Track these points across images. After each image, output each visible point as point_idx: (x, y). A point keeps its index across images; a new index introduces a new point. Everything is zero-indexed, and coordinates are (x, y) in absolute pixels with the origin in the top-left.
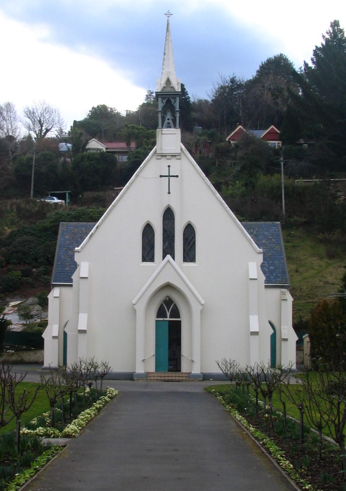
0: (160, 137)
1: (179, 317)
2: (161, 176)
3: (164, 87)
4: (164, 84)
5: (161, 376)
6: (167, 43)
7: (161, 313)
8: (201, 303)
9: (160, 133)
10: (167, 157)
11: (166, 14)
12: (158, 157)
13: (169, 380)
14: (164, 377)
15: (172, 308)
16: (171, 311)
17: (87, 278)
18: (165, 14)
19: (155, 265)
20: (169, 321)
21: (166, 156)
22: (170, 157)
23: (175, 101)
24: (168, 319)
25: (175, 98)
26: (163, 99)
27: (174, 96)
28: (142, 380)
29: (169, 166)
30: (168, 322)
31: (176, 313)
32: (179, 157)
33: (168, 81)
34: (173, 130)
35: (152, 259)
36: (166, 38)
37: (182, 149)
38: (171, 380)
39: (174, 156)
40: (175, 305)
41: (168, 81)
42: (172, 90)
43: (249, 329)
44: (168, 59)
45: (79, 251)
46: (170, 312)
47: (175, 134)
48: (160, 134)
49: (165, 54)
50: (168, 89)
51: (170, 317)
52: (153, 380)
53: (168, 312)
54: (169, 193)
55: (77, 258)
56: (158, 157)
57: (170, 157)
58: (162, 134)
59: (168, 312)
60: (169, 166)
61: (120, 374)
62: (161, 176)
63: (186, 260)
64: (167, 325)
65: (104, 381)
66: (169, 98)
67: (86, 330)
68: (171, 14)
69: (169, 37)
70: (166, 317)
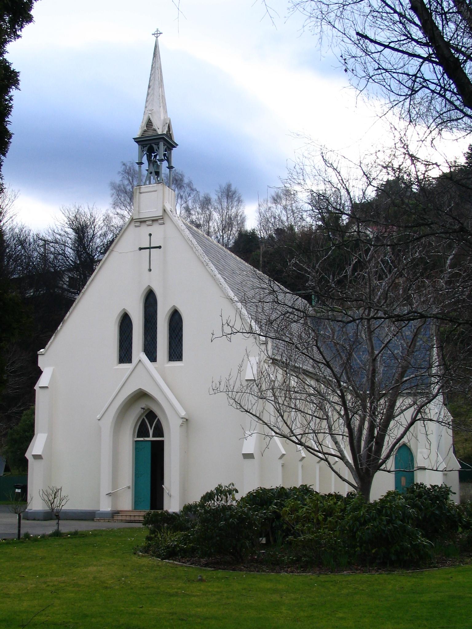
0: (137, 196)
1: (163, 436)
2: (141, 249)
3: (145, 131)
4: (144, 127)
5: (131, 516)
6: (153, 72)
7: (142, 431)
8: (179, 416)
9: (138, 191)
10: (147, 223)
11: (154, 34)
12: (136, 224)
13: (136, 521)
14: (129, 517)
15: (156, 424)
16: (155, 427)
17: (47, 387)
18: (153, 34)
19: (183, 365)
20: (152, 441)
21: (145, 221)
22: (151, 223)
23: (158, 148)
24: (151, 439)
25: (158, 144)
26: (144, 147)
27: (157, 141)
28: (103, 521)
29: (150, 235)
30: (150, 443)
31: (159, 431)
32: (162, 222)
33: (149, 123)
34: (154, 186)
35: (129, 361)
36: (152, 66)
37: (166, 211)
38: (138, 521)
39: (154, 220)
40: (159, 421)
41: (149, 123)
42: (155, 133)
43: (241, 450)
44: (153, 94)
45: (43, 353)
46: (154, 430)
47: (156, 191)
48: (138, 193)
49: (149, 87)
50: (150, 133)
51: (153, 436)
52: (116, 521)
53: (151, 429)
54: (150, 270)
55: (42, 362)
56: (136, 224)
57: (139, 224)
58: (140, 193)
59: (151, 429)
60: (150, 235)
61: (82, 512)
62: (141, 249)
63: (172, 358)
64: (149, 445)
65: (60, 522)
66: (150, 144)
67: (252, 454)
68: (160, 33)
69: (155, 65)
70: (149, 436)
